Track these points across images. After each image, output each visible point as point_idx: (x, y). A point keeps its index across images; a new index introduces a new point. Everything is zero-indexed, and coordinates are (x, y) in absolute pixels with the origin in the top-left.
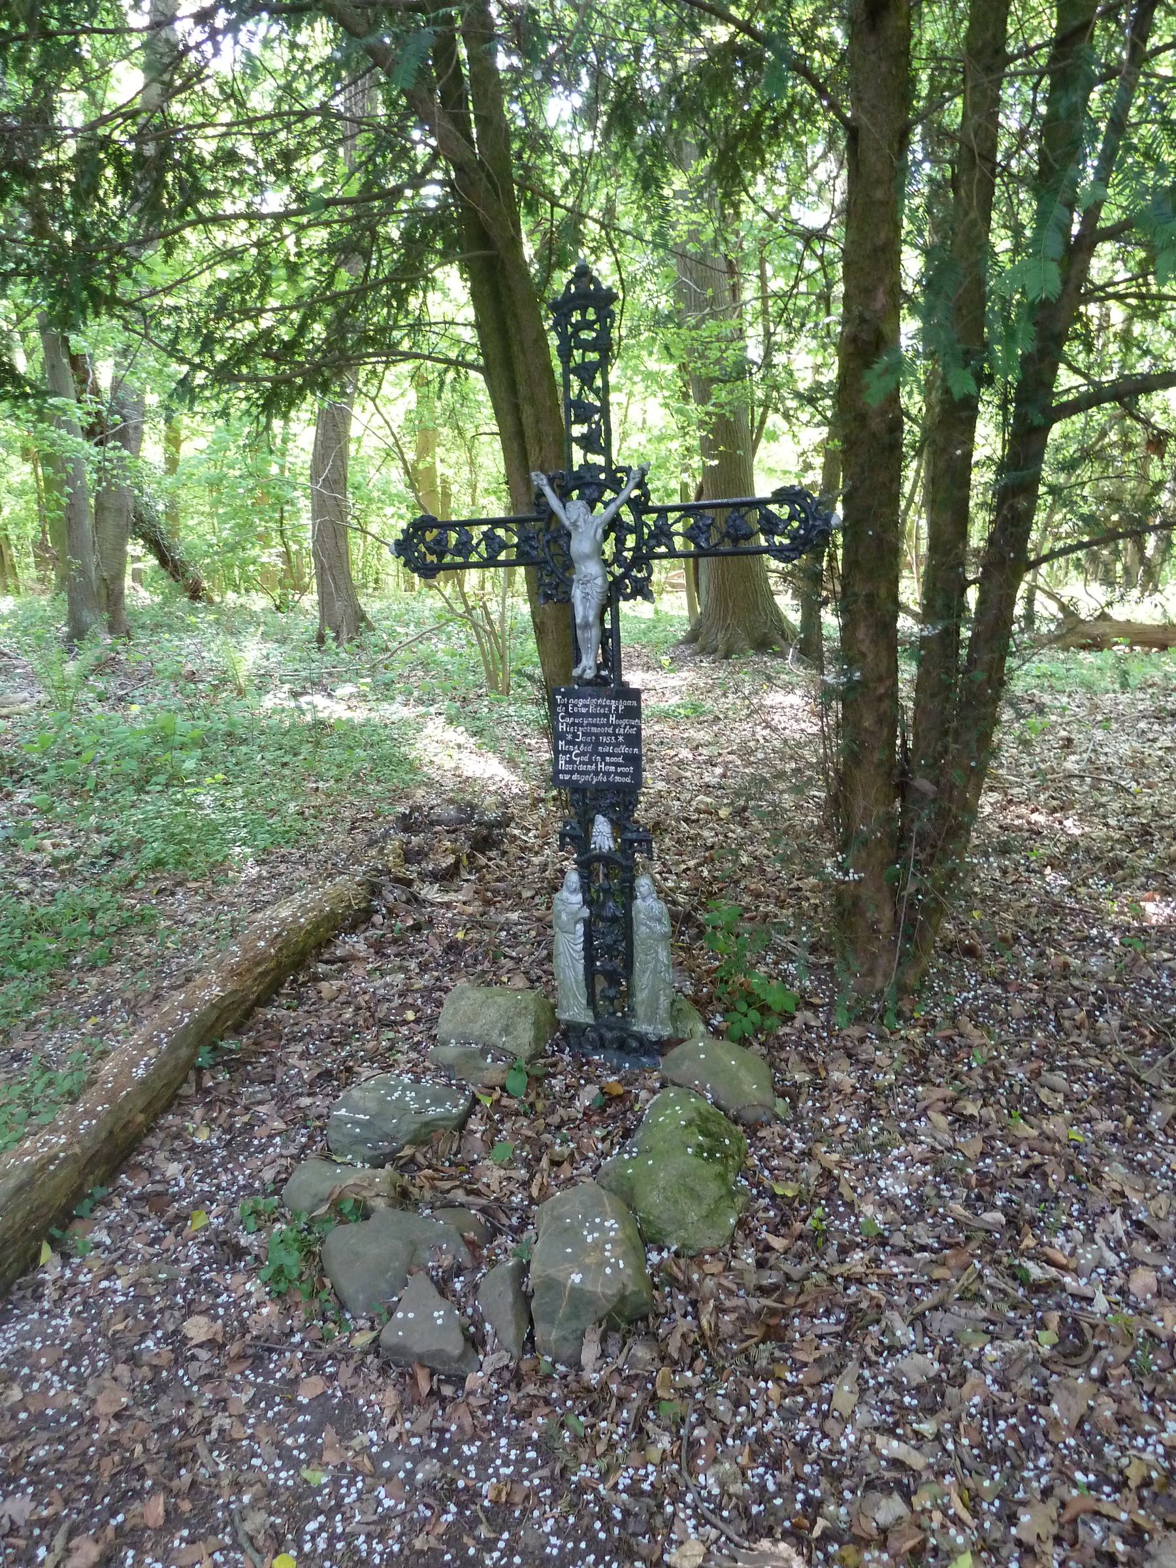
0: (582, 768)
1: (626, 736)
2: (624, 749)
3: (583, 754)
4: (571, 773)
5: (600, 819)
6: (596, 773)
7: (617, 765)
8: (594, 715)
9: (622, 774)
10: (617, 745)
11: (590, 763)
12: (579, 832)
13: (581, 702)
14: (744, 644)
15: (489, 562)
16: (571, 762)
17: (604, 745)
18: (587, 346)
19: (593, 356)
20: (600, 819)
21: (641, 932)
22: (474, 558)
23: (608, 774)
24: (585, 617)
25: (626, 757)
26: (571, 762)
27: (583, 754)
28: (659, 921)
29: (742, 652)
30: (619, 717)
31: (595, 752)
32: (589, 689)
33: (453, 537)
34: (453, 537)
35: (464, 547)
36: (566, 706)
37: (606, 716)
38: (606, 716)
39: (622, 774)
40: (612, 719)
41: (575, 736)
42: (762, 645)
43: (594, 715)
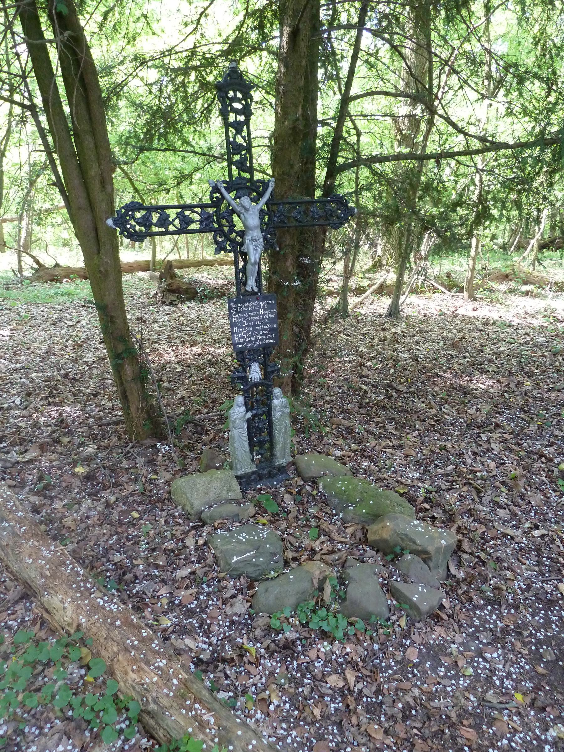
0: (248, 339)
2: (269, 326)
3: (248, 332)
5: (277, 391)
6: (256, 341)
7: (266, 334)
8: (251, 311)
9: (269, 339)
10: (265, 324)
11: (252, 336)
13: (244, 305)
15: (182, 231)
17: (258, 325)
18: (237, 112)
19: (242, 118)
20: (277, 391)
21: (277, 415)
22: (171, 228)
23: (262, 340)
27: (248, 332)
28: (286, 407)
30: (265, 310)
31: (254, 330)
33: (155, 217)
34: (155, 217)
35: (164, 221)
36: (236, 308)
37: (258, 310)
39: (269, 339)
40: (262, 311)
41: (242, 323)
43: (251, 311)
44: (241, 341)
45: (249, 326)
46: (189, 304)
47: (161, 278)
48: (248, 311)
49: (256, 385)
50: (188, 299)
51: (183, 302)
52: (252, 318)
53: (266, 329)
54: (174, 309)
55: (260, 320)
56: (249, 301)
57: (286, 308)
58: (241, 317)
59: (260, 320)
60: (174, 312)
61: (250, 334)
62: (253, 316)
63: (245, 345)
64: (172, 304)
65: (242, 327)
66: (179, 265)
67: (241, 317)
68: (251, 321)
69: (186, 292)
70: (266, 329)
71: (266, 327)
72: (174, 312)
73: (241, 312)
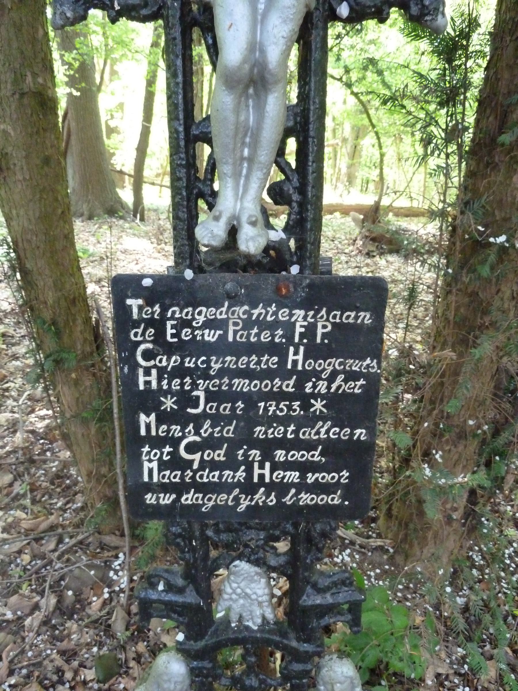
0: (207, 477)
1: (334, 400)
2: (324, 430)
3: (211, 443)
4: (179, 489)
6: (249, 488)
7: (304, 468)
8: (249, 349)
9: (318, 488)
10: (310, 420)
11: (232, 464)
12: (191, 597)
13: (203, 314)
14: (100, 211)
16: (176, 463)
17: (270, 421)
23: (282, 489)
24: (255, 47)
25: (330, 448)
26: (176, 463)
27: (211, 443)
29: (99, 216)
30: (314, 352)
32: (229, 282)
36: (158, 325)
37: (279, 350)
38: (273, 349)
39: (318, 488)
40: (296, 357)
41: (186, 399)
42: (112, 212)
43: (249, 349)
44: (174, 476)
45: (217, 419)
46: (390, 258)
47: (363, 221)
48: (221, 348)
49: (243, 639)
50: (391, 252)
51: (381, 254)
52: (241, 385)
53: (310, 446)
54: (369, 261)
55: (280, 396)
56: (234, 299)
57: (486, 312)
58: (180, 372)
59: (280, 396)
60: (367, 265)
61: (219, 455)
62: (247, 374)
63: (189, 498)
64: (369, 255)
65: (179, 417)
66: (408, 213)
67: (180, 372)
68: (232, 396)
69: (390, 242)
70: (310, 446)
71: (307, 434)
72: (367, 265)
73: (181, 348)
